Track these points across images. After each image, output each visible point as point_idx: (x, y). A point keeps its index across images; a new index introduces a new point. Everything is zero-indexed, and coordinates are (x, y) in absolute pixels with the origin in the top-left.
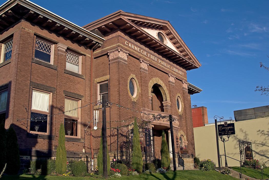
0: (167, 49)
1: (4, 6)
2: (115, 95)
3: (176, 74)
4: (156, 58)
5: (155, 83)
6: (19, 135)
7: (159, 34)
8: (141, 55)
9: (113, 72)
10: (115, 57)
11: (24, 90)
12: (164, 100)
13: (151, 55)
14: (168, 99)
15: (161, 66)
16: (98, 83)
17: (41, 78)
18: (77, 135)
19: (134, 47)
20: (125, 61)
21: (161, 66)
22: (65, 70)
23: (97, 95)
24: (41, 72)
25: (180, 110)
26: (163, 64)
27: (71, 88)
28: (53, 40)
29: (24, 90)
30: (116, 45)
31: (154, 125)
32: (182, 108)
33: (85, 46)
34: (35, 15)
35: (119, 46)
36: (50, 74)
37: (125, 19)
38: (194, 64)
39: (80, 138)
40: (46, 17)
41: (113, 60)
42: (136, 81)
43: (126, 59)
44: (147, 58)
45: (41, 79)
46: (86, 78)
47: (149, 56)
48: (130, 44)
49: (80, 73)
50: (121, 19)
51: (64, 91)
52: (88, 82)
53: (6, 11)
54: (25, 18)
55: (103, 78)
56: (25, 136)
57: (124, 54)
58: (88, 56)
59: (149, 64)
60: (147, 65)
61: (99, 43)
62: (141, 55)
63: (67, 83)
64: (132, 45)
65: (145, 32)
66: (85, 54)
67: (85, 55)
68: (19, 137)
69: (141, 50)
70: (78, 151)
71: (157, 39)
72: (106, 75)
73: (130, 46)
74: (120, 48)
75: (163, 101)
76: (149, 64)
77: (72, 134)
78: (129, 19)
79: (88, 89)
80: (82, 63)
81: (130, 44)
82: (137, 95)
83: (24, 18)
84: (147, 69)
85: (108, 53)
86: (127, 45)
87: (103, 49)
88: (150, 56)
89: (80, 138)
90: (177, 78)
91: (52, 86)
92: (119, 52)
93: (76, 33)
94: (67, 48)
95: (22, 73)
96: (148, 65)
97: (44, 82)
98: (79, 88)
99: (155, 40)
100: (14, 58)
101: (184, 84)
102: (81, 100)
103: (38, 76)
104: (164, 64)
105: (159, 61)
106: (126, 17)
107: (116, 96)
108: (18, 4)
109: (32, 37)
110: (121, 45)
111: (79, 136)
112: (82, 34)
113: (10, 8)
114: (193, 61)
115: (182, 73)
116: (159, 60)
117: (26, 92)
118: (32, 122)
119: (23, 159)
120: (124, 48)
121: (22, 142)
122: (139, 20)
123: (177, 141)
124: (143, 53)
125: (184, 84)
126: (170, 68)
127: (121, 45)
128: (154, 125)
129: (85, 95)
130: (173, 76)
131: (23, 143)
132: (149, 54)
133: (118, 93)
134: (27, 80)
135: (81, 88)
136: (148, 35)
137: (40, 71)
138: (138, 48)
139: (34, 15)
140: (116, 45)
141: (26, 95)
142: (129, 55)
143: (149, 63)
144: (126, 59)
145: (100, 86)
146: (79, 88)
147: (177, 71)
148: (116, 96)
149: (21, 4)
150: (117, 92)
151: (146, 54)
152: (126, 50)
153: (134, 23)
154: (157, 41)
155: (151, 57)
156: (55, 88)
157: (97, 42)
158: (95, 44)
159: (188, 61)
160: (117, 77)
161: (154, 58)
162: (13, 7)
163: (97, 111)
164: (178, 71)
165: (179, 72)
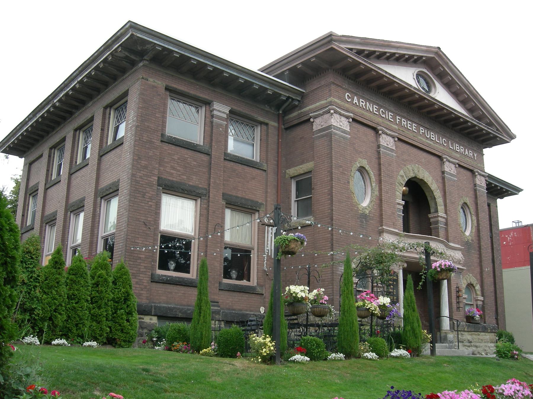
0: (436, 107)
1: (110, 41)
2: (323, 201)
3: (458, 156)
4: (414, 124)
5: (412, 175)
6: (137, 277)
7: (419, 75)
8: (380, 120)
9: (321, 156)
10: (323, 127)
11: (147, 194)
12: (432, 210)
13: (403, 120)
14: (441, 208)
15: (424, 140)
16: (291, 178)
17: (179, 171)
18: (249, 280)
19: (364, 104)
20: (344, 132)
21: (424, 140)
22: (226, 154)
23: (291, 201)
24: (179, 159)
25: (467, 233)
26: (428, 137)
27: (239, 188)
28: (201, 98)
29: (147, 194)
30: (325, 101)
31: (406, 262)
32: (472, 227)
33: (266, 106)
34: (166, 52)
35: (331, 103)
36: (195, 163)
37: (342, 48)
38: (499, 134)
39: (255, 284)
40: (186, 54)
41: (320, 131)
42: (368, 174)
43: (348, 129)
44: (393, 126)
45: (178, 173)
46: (267, 167)
47: (398, 120)
48: (355, 98)
49: (257, 158)
50: (332, 49)
51: (224, 194)
52: (272, 177)
53: (114, 49)
54: (148, 59)
55: (301, 168)
56: (148, 279)
57: (343, 119)
58: (272, 126)
59: (398, 138)
60: (392, 140)
61: (293, 99)
62: (380, 120)
63: (230, 179)
64: (361, 100)
65: (386, 72)
66: (266, 121)
67: (267, 124)
68: (137, 280)
69: (381, 110)
70: (251, 311)
71: (417, 88)
72: (308, 161)
73: (357, 102)
74: (334, 107)
75: (430, 213)
76: (398, 138)
77: (240, 278)
78: (351, 49)
79: (272, 191)
80: (261, 140)
81: (355, 98)
82: (371, 202)
83: (145, 60)
84: (394, 148)
85: (311, 117)
86: (349, 100)
87: (302, 111)
88: (401, 122)
89: (255, 284)
90: (462, 164)
91: (200, 186)
92: (332, 114)
93: (246, 81)
94: (230, 111)
95: (142, 162)
96: (396, 139)
97: (185, 177)
98: (254, 188)
99: (409, 88)
100: (129, 135)
101: (478, 177)
102: (258, 211)
103: (173, 168)
104: (432, 136)
105: (421, 131)
106: (343, 46)
107: (326, 203)
108: (132, 35)
109: (161, 93)
110: (336, 100)
111: (254, 281)
112: (258, 83)
113: (120, 43)
114: (497, 130)
115: (473, 155)
116: (421, 128)
117: (150, 198)
118: (162, 253)
119: (143, 320)
120: (342, 108)
121: (142, 290)
122: (372, 49)
123: (458, 297)
124: (384, 116)
125: (478, 177)
126: (445, 145)
127: (336, 100)
128: (406, 262)
129: (266, 201)
130: (451, 160)
131: (142, 292)
132: (398, 117)
133: (329, 197)
134: (151, 174)
135: (259, 189)
136: (392, 78)
137: (176, 157)
138: (374, 106)
139: (164, 53)
140: (325, 101)
141: (150, 203)
142: (354, 120)
143: (397, 134)
144: (348, 129)
145: (298, 183)
146: (254, 188)
147: (461, 150)
148: (326, 203)
149: (138, 35)
150: (327, 195)
151: (390, 117)
152: (347, 111)
153: (363, 55)
154: (412, 89)
155: (403, 123)
156: (206, 190)
157: (288, 98)
158: (284, 102)
159: (486, 129)
160: (327, 165)
161: (409, 125)
162: (124, 41)
163: (432, 218)
164: (463, 150)
165: (467, 153)
